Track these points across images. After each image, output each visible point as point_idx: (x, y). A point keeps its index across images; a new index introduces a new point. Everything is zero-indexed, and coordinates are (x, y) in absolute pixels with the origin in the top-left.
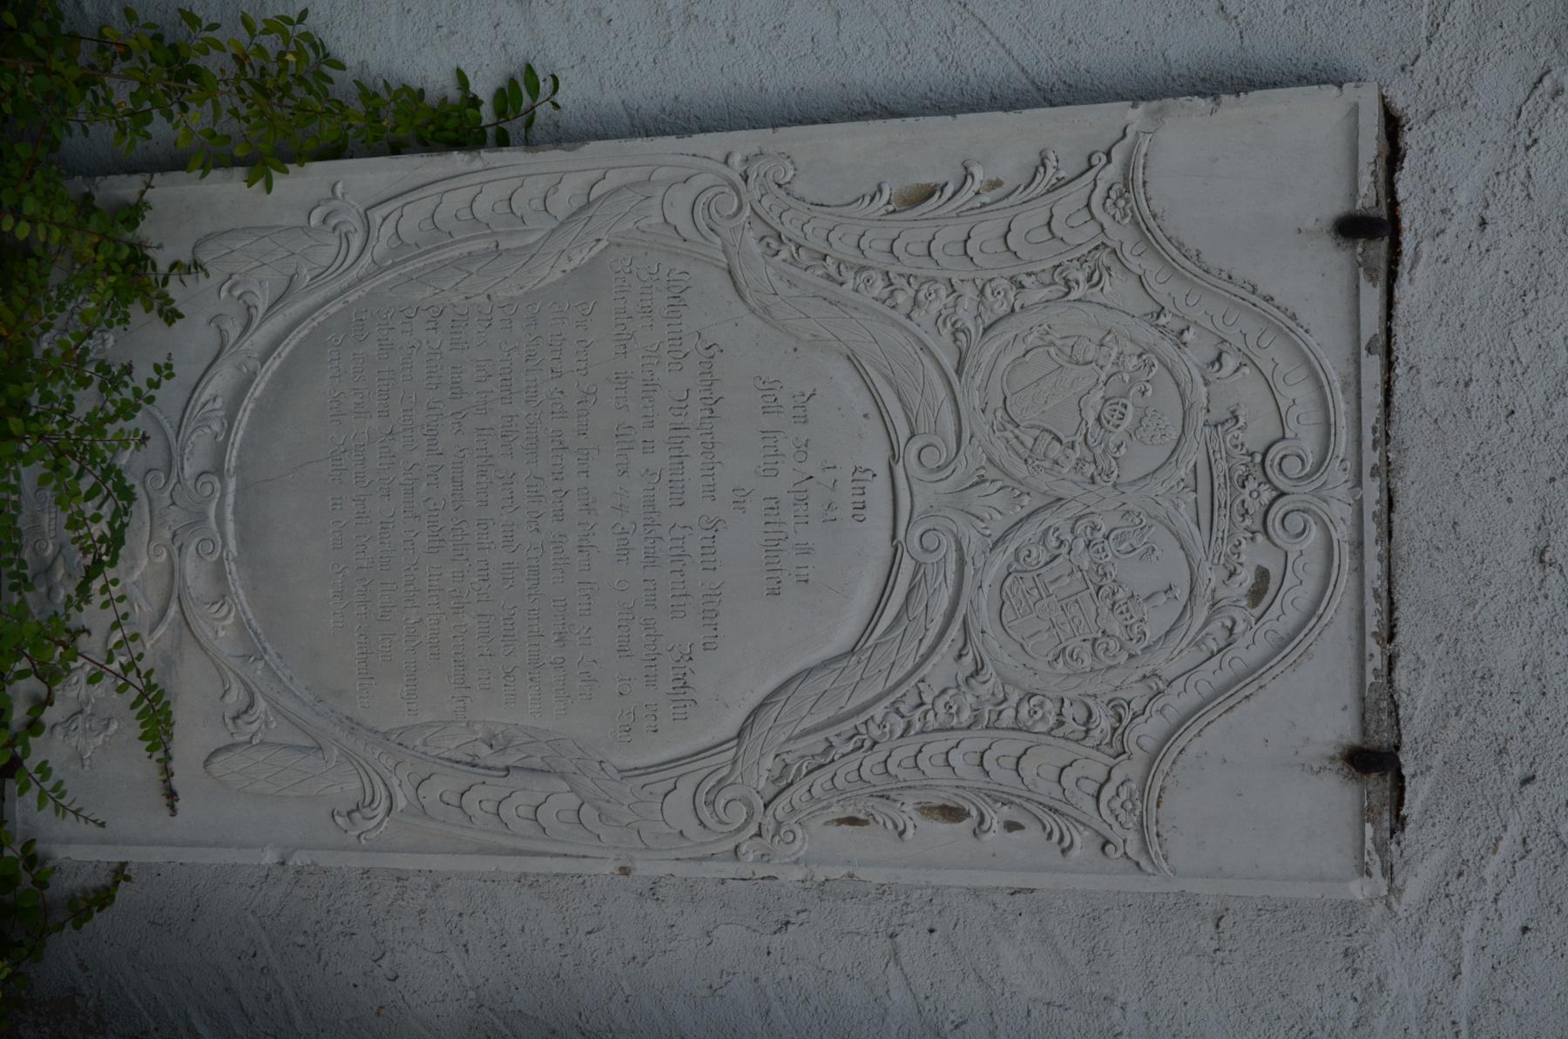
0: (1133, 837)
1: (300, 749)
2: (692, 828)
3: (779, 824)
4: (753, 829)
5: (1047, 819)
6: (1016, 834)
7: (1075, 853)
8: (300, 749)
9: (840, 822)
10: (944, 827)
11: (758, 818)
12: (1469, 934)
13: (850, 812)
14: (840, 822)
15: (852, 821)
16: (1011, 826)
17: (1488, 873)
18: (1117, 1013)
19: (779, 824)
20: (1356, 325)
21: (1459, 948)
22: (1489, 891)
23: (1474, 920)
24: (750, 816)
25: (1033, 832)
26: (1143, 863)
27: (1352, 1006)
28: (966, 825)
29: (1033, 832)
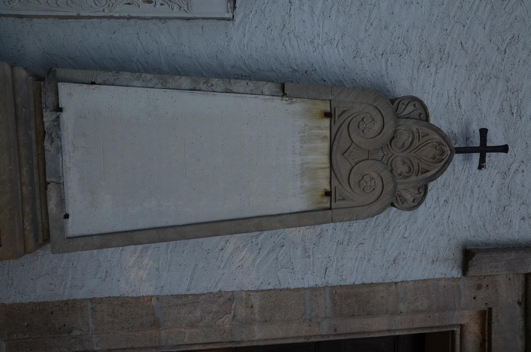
0: (185, 6)
1: (334, 171)
2: (94, 5)
3: (113, 4)
4: (107, 5)
5: (169, 3)
6: (163, 6)
7: (175, 9)
8: (334, 171)
9: (126, 4)
10: (148, 5)
11: (108, 3)
12: (247, 28)
13: (128, 2)
14: (126, 4)
15: (129, 4)
16: (162, 4)
17: (250, 17)
18: (183, 47)
19: (113, 4)
20: (268, 99)
21: (245, 31)
22: (250, 20)
23: (248, 25)
24: (106, 3)
25: (166, 6)
26: (188, 11)
27: (227, 43)
28: (153, 4)
29: (166, 6)
